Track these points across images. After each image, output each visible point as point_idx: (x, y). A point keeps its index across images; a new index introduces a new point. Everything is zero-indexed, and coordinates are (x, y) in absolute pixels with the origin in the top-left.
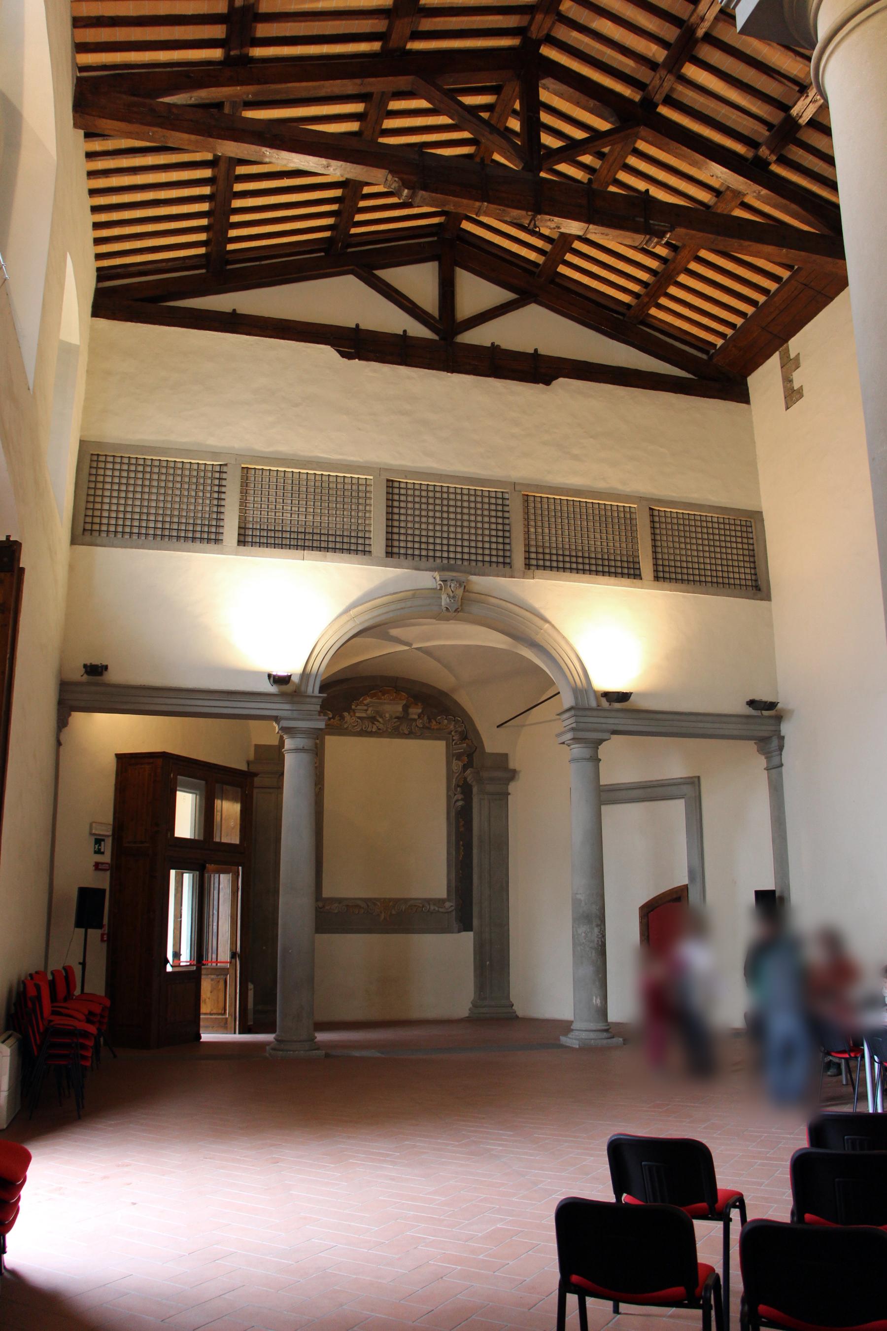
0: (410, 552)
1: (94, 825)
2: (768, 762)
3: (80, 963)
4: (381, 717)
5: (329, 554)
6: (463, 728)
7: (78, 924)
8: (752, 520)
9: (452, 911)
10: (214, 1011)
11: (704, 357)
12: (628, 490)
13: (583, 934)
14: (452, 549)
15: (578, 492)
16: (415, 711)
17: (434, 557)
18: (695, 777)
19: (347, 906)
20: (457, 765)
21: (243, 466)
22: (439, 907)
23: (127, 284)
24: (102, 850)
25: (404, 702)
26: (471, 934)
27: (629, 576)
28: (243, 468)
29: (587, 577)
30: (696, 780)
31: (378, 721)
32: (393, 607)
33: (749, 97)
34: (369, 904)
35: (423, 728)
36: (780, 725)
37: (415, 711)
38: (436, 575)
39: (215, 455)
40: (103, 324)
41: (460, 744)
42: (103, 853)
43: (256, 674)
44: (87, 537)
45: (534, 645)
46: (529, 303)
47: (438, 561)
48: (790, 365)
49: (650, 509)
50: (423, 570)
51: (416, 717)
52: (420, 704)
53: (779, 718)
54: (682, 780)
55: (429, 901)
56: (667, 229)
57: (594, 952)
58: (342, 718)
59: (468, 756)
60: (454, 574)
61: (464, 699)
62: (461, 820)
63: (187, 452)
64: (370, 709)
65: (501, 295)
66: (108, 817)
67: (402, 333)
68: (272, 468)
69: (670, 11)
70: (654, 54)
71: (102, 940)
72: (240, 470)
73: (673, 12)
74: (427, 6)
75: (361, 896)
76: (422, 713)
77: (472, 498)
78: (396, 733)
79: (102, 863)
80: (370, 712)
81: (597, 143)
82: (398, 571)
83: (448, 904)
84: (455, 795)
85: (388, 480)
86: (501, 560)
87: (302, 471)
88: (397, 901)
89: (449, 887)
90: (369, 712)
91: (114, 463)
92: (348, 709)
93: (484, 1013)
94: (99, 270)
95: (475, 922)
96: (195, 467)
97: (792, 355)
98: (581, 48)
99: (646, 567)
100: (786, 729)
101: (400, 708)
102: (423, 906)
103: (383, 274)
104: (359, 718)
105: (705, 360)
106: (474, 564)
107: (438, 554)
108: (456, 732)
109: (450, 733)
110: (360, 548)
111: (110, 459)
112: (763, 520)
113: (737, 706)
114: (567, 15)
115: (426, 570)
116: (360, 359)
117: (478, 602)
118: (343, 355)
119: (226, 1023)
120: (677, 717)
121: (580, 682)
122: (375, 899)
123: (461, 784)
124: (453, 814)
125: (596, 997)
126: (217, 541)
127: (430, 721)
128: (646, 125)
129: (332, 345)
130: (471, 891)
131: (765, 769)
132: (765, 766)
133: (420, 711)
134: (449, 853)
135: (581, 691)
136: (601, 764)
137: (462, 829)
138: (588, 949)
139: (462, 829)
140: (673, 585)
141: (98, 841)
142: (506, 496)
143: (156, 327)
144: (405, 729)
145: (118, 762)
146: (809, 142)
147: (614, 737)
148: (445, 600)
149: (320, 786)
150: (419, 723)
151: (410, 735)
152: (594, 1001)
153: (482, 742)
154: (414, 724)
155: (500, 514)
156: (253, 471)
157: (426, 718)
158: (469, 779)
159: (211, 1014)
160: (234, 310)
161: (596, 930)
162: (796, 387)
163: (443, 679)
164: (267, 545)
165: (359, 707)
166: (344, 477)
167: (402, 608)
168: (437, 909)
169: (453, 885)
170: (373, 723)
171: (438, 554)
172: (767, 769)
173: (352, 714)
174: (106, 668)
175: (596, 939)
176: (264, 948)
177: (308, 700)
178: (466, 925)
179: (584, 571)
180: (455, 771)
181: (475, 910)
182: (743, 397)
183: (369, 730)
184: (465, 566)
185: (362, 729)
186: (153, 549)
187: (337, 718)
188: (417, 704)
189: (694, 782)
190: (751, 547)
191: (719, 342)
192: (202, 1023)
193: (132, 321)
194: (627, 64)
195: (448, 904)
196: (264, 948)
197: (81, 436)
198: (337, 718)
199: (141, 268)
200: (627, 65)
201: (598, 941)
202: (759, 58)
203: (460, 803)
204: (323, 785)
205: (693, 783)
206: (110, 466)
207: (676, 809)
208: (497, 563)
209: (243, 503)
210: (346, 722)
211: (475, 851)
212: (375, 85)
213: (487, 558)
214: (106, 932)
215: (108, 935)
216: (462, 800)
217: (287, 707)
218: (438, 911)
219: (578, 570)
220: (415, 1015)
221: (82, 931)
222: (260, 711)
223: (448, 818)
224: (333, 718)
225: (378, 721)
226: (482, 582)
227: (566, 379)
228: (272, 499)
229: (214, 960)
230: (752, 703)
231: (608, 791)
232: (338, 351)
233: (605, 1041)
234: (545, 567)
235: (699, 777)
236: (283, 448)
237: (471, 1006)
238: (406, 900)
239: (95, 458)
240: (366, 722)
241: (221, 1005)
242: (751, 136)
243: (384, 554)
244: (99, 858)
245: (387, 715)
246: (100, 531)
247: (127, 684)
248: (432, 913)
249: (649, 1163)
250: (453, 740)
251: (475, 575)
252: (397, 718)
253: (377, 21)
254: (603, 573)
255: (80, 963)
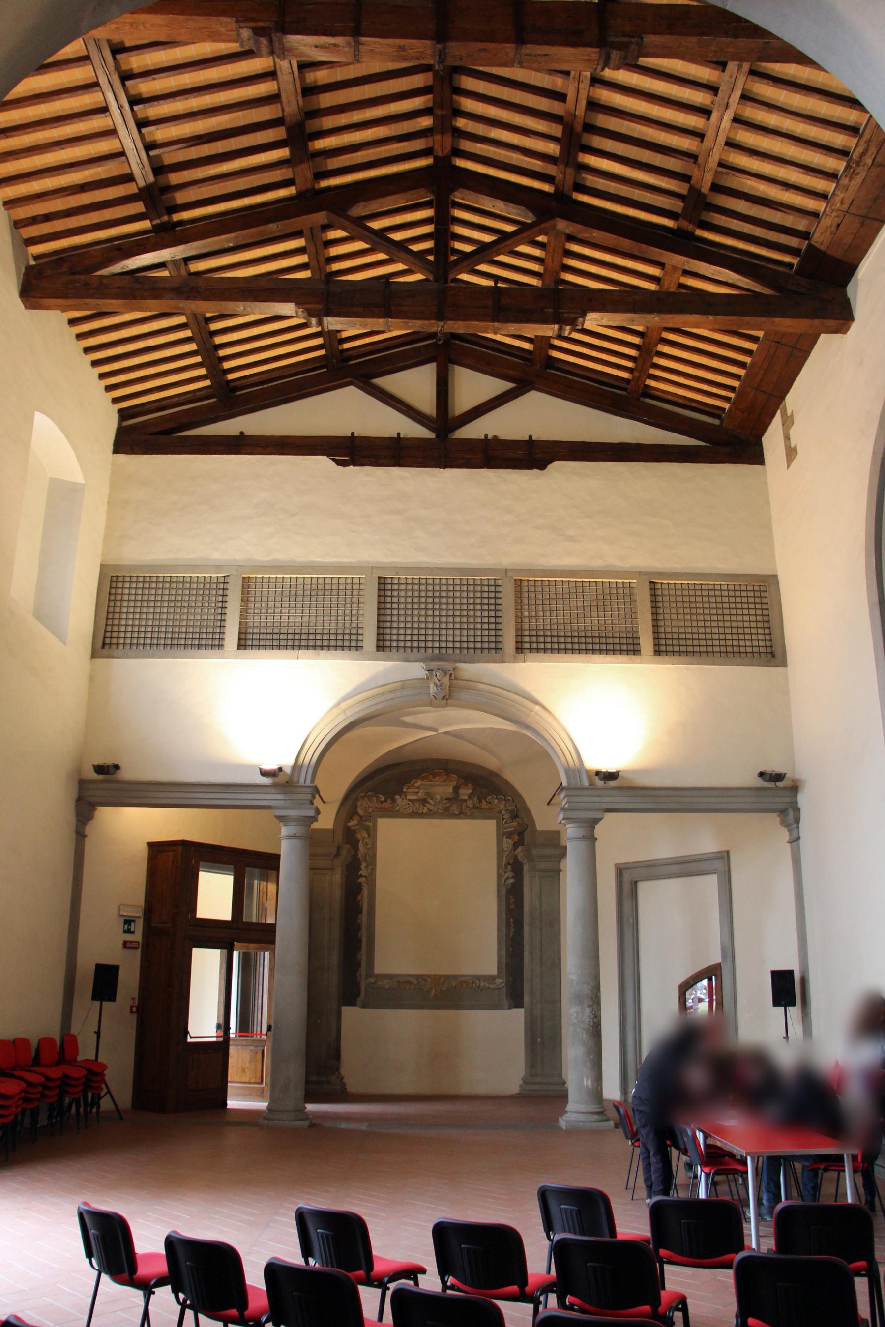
0: (402, 644)
1: (122, 907)
2: (790, 834)
3: (95, 1032)
4: (432, 798)
5: (322, 653)
6: (514, 807)
7: (94, 998)
8: (766, 584)
9: (503, 988)
10: (253, 1080)
11: (717, 422)
12: (627, 565)
13: (575, 1015)
14: (443, 638)
15: (573, 573)
16: (465, 792)
17: (426, 647)
18: (724, 851)
19: (398, 982)
20: (508, 843)
21: (243, 575)
22: (489, 984)
23: (145, 421)
24: (132, 930)
25: (454, 784)
26: (522, 1010)
27: (628, 652)
28: (244, 578)
29: (582, 656)
30: (725, 854)
31: (429, 803)
32: (383, 698)
33: (654, 175)
34: (420, 980)
35: (473, 808)
36: (796, 796)
37: (465, 792)
38: (422, 664)
39: (218, 567)
40: (122, 458)
41: (510, 822)
42: (133, 933)
43: (249, 767)
44: (106, 651)
45: (528, 727)
46: (529, 391)
47: (430, 651)
48: (788, 422)
49: (651, 582)
50: (412, 661)
51: (466, 797)
52: (470, 785)
53: (795, 789)
54: (713, 855)
55: (479, 978)
56: (577, 315)
57: (585, 1032)
58: (394, 801)
59: (519, 834)
60: (440, 663)
61: (512, 777)
62: (511, 897)
63: (194, 567)
64: (421, 791)
65: (495, 386)
66: (139, 898)
67: (396, 436)
68: (272, 576)
69: (551, 111)
70: (554, 151)
71: (131, 1012)
72: (241, 580)
73: (555, 112)
74: (327, 149)
75: (412, 972)
76: (472, 793)
77: (465, 588)
78: (447, 814)
79: (131, 942)
80: (421, 794)
81: (508, 243)
82: (389, 664)
83: (498, 981)
84: (506, 872)
85: (379, 578)
86: (493, 645)
87: (299, 576)
88: (447, 977)
89: (499, 963)
90: (420, 794)
91: (130, 582)
92: (400, 792)
93: (535, 1090)
94: (120, 411)
95: (526, 998)
96: (202, 580)
97: (789, 414)
98: (490, 156)
99: (646, 642)
100: (803, 800)
101: (451, 790)
102: (473, 983)
103: (380, 382)
104: (410, 800)
105: (716, 425)
106: (458, 651)
107: (430, 644)
108: (506, 810)
109: (500, 812)
110: (354, 644)
111: (134, 579)
112: (778, 584)
113: (747, 778)
114: (466, 130)
115: (416, 661)
116: (354, 465)
117: (469, 689)
118: (339, 463)
119: (262, 1092)
120: (679, 793)
121: (572, 762)
122: (427, 975)
123: (511, 862)
124: (504, 891)
125: (587, 1079)
126: (220, 646)
127: (480, 802)
128: (561, 217)
129: (328, 455)
130: (522, 968)
131: (788, 842)
132: (787, 839)
133: (470, 791)
134: (499, 930)
135: (573, 771)
136: (597, 843)
137: (513, 906)
138: (579, 1030)
139: (513, 906)
140: (677, 658)
141: (128, 922)
142: (500, 583)
143: (169, 456)
144: (455, 809)
145: (149, 849)
146: (727, 207)
147: (609, 816)
148: (432, 689)
149: (372, 867)
150: (470, 803)
151: (461, 815)
152: (585, 1083)
153: (533, 821)
154: (464, 804)
155: (492, 601)
156: (254, 579)
157: (476, 798)
158: (520, 857)
159: (250, 1083)
160: (242, 433)
161: (588, 1011)
162: (792, 446)
163: (490, 762)
164: (265, 647)
165: (410, 790)
166: (346, 578)
167: (392, 699)
168: (487, 985)
169: (504, 960)
170: (424, 805)
171: (430, 644)
172: (790, 842)
173: (403, 797)
174: (117, 767)
175: (587, 1020)
176: (319, 1021)
177: (300, 790)
178: (517, 1002)
179: (580, 651)
180: (505, 849)
181: (526, 986)
182: (756, 457)
183: (420, 812)
184: (450, 654)
185: (413, 811)
186: (161, 657)
187: (389, 801)
188: (467, 785)
189: (724, 857)
190: (765, 612)
191: (727, 406)
192: (229, 1092)
193: (147, 454)
194: (536, 165)
195: (498, 981)
196: (319, 1021)
197: (102, 561)
198: (389, 801)
199: (156, 404)
200: (536, 164)
201: (589, 1022)
202: (648, 139)
203: (511, 881)
204: (375, 866)
205: (722, 858)
206: (127, 585)
207: (710, 884)
208: (489, 649)
209: (244, 611)
210: (398, 805)
211: (526, 928)
212: (305, 221)
213: (479, 645)
214: (136, 1004)
215: (138, 1007)
216: (513, 877)
217: (280, 797)
218: (489, 988)
219: (587, 651)
220: (466, 1090)
221: (98, 1003)
222: (253, 801)
223: (499, 896)
224: (385, 801)
225: (429, 803)
226: (469, 669)
227: (562, 462)
228: (271, 604)
229: (259, 1032)
230: (761, 774)
231: (646, 867)
232: (334, 460)
233: (594, 1124)
234: (538, 650)
235: (728, 852)
236: (282, 556)
237: (521, 1082)
238: (455, 977)
239: (115, 579)
240: (417, 804)
241: (259, 1075)
242: (672, 210)
243: (374, 648)
244: (129, 937)
245: (438, 797)
246: (117, 644)
247: (137, 780)
248: (482, 990)
249: (470, 1246)
250: (504, 819)
251: (464, 662)
252: (447, 799)
253: (284, 170)
254: (600, 651)
255: (95, 1032)
